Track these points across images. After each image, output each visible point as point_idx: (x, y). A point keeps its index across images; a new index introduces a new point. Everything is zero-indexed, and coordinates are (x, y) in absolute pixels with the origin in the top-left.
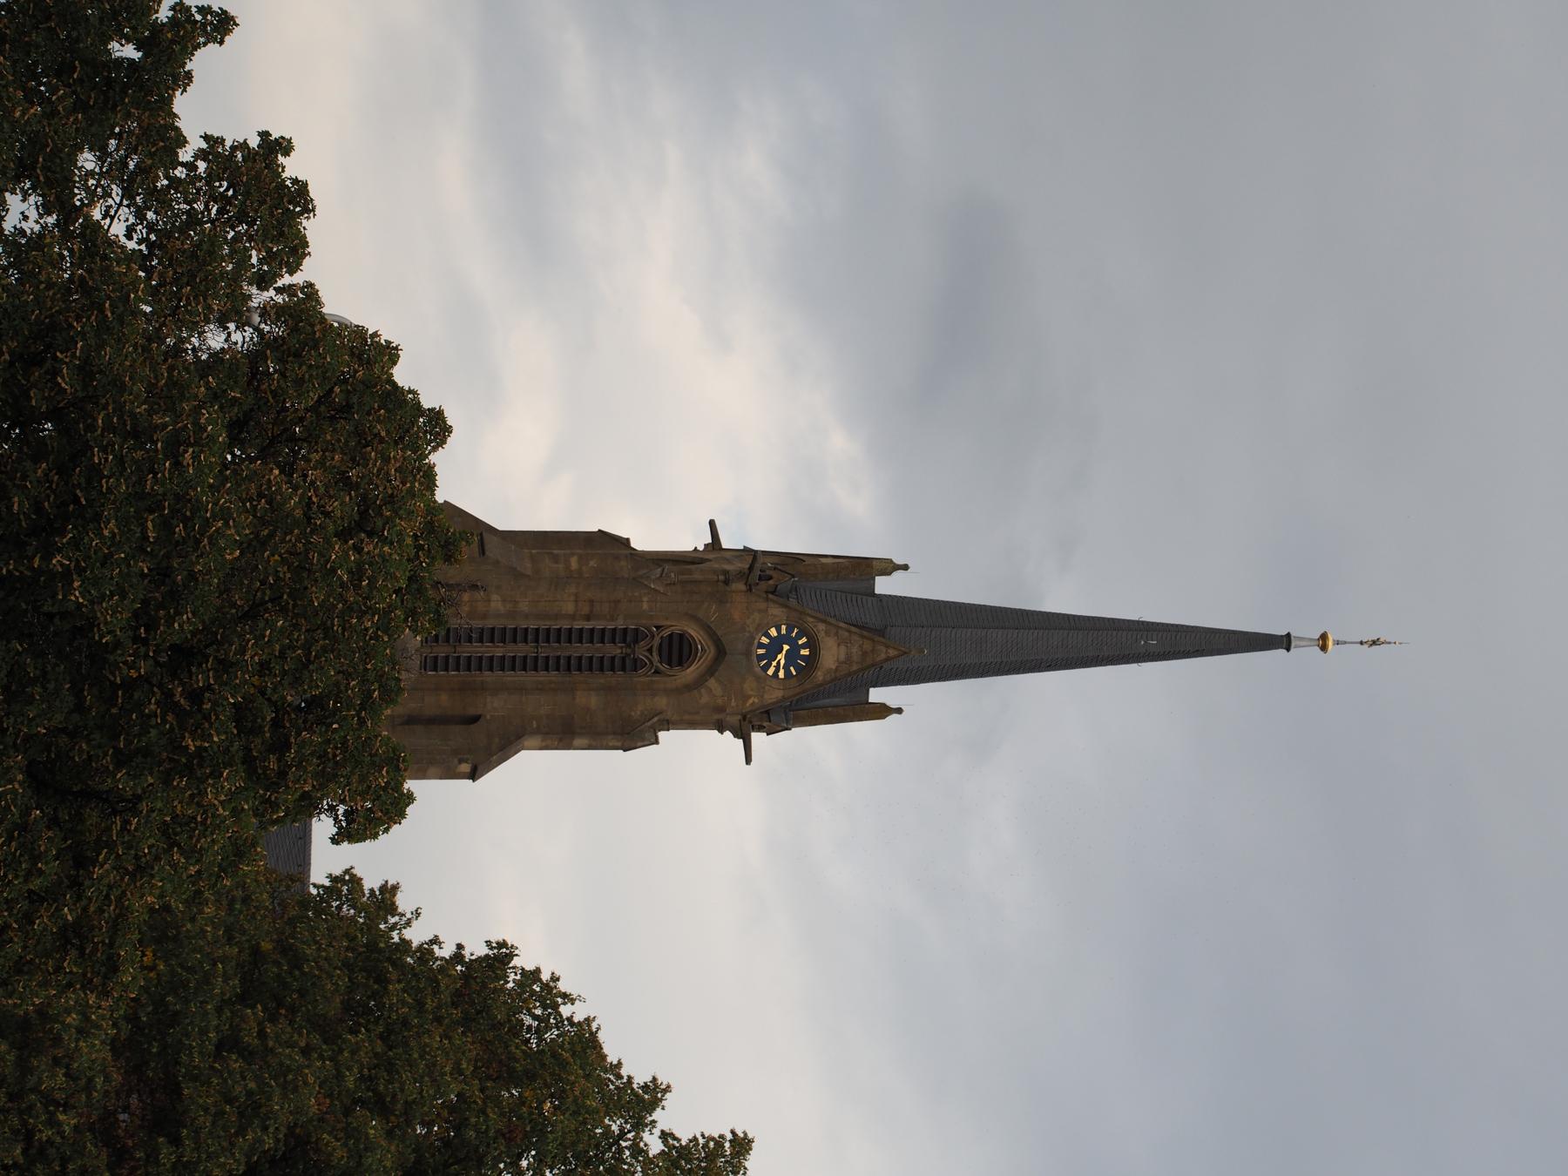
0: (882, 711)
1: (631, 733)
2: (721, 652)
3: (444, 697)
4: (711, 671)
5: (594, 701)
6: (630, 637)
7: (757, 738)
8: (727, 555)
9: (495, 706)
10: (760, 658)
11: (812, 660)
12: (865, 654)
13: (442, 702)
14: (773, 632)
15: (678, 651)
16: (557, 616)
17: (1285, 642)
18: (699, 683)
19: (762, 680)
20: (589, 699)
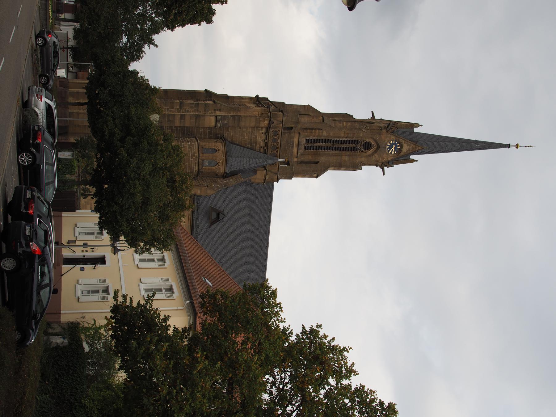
0: (413, 161)
1: (356, 167)
2: (378, 147)
3: (310, 157)
4: (376, 151)
5: (347, 158)
6: (356, 142)
7: (386, 168)
8: (378, 121)
9: (322, 159)
10: (388, 148)
11: (400, 150)
12: (413, 148)
13: (310, 158)
14: (391, 142)
15: (367, 146)
16: (340, 137)
17: (509, 146)
18: (373, 154)
19: (388, 154)
20: (345, 157)
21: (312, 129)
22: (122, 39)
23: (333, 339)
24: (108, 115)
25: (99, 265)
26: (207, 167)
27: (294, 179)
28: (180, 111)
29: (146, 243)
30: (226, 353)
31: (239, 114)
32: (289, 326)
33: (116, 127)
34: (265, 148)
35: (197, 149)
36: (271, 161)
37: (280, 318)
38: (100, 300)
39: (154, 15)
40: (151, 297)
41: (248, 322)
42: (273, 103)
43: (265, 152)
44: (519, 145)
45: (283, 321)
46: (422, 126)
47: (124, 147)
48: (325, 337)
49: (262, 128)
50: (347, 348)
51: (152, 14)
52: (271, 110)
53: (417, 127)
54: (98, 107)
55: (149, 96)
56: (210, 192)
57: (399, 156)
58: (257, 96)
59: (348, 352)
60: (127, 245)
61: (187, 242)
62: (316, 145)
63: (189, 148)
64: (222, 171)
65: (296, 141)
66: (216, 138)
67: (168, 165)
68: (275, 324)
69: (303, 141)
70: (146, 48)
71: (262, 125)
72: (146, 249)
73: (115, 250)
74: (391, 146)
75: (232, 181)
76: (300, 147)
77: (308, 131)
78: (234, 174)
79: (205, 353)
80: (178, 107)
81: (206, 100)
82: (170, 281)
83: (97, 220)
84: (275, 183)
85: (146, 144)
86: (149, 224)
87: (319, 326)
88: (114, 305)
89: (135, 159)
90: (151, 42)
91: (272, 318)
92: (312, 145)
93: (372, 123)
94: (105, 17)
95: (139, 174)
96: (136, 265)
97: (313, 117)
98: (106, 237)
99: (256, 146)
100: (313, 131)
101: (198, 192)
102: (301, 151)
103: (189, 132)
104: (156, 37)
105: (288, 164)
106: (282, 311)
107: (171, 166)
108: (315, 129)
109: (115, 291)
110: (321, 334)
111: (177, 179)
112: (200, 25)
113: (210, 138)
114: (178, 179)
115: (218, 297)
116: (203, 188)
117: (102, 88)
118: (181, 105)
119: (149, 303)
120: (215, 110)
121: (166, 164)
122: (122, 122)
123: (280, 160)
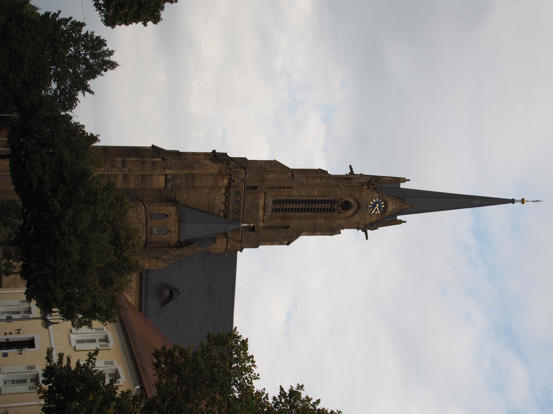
0: (400, 222)
1: (333, 231)
2: (359, 206)
3: (279, 221)
4: (356, 212)
5: (323, 221)
7: (369, 231)
9: (294, 223)
11: (385, 209)
12: (400, 207)
13: (279, 222)
14: (374, 201)
15: (346, 206)
17: (513, 201)
18: (353, 215)
19: (370, 214)
21: (280, 188)
22: (50, 85)
23: (318, 401)
25: (26, 349)
27: (260, 247)
29: (85, 315)
31: (193, 172)
32: (264, 389)
34: (226, 212)
35: (144, 214)
36: (232, 227)
37: (253, 374)
38: (28, 391)
39: (88, 57)
40: (94, 355)
42: (233, 159)
43: (226, 216)
44: (526, 199)
46: (409, 180)
47: (56, 197)
48: (308, 399)
49: (221, 188)
51: (86, 55)
52: (231, 167)
54: (23, 159)
57: (384, 216)
60: (62, 318)
61: (135, 320)
63: (136, 216)
64: (175, 239)
65: (261, 202)
67: (111, 218)
68: (246, 381)
69: (270, 202)
71: (221, 184)
73: (47, 324)
74: (374, 206)
75: (187, 251)
76: (266, 209)
77: (276, 190)
78: (189, 243)
80: (120, 166)
81: (154, 157)
83: (8, 162)
84: (239, 252)
87: (301, 387)
88: (48, 367)
89: (70, 210)
90: (86, 89)
91: (243, 375)
92: (281, 207)
93: (351, 179)
94: (29, 59)
96: (73, 347)
97: (281, 173)
98: (36, 311)
99: (214, 209)
100: (282, 190)
101: (147, 265)
102: (268, 214)
103: (134, 195)
105: (253, 229)
106: (254, 366)
108: (284, 188)
110: (303, 396)
111: (122, 234)
112: (145, 25)
114: (123, 234)
115: (177, 354)
116: (152, 261)
118: (124, 163)
119: (91, 362)
120: (164, 168)
121: (108, 217)
122: (53, 169)
123: (244, 225)
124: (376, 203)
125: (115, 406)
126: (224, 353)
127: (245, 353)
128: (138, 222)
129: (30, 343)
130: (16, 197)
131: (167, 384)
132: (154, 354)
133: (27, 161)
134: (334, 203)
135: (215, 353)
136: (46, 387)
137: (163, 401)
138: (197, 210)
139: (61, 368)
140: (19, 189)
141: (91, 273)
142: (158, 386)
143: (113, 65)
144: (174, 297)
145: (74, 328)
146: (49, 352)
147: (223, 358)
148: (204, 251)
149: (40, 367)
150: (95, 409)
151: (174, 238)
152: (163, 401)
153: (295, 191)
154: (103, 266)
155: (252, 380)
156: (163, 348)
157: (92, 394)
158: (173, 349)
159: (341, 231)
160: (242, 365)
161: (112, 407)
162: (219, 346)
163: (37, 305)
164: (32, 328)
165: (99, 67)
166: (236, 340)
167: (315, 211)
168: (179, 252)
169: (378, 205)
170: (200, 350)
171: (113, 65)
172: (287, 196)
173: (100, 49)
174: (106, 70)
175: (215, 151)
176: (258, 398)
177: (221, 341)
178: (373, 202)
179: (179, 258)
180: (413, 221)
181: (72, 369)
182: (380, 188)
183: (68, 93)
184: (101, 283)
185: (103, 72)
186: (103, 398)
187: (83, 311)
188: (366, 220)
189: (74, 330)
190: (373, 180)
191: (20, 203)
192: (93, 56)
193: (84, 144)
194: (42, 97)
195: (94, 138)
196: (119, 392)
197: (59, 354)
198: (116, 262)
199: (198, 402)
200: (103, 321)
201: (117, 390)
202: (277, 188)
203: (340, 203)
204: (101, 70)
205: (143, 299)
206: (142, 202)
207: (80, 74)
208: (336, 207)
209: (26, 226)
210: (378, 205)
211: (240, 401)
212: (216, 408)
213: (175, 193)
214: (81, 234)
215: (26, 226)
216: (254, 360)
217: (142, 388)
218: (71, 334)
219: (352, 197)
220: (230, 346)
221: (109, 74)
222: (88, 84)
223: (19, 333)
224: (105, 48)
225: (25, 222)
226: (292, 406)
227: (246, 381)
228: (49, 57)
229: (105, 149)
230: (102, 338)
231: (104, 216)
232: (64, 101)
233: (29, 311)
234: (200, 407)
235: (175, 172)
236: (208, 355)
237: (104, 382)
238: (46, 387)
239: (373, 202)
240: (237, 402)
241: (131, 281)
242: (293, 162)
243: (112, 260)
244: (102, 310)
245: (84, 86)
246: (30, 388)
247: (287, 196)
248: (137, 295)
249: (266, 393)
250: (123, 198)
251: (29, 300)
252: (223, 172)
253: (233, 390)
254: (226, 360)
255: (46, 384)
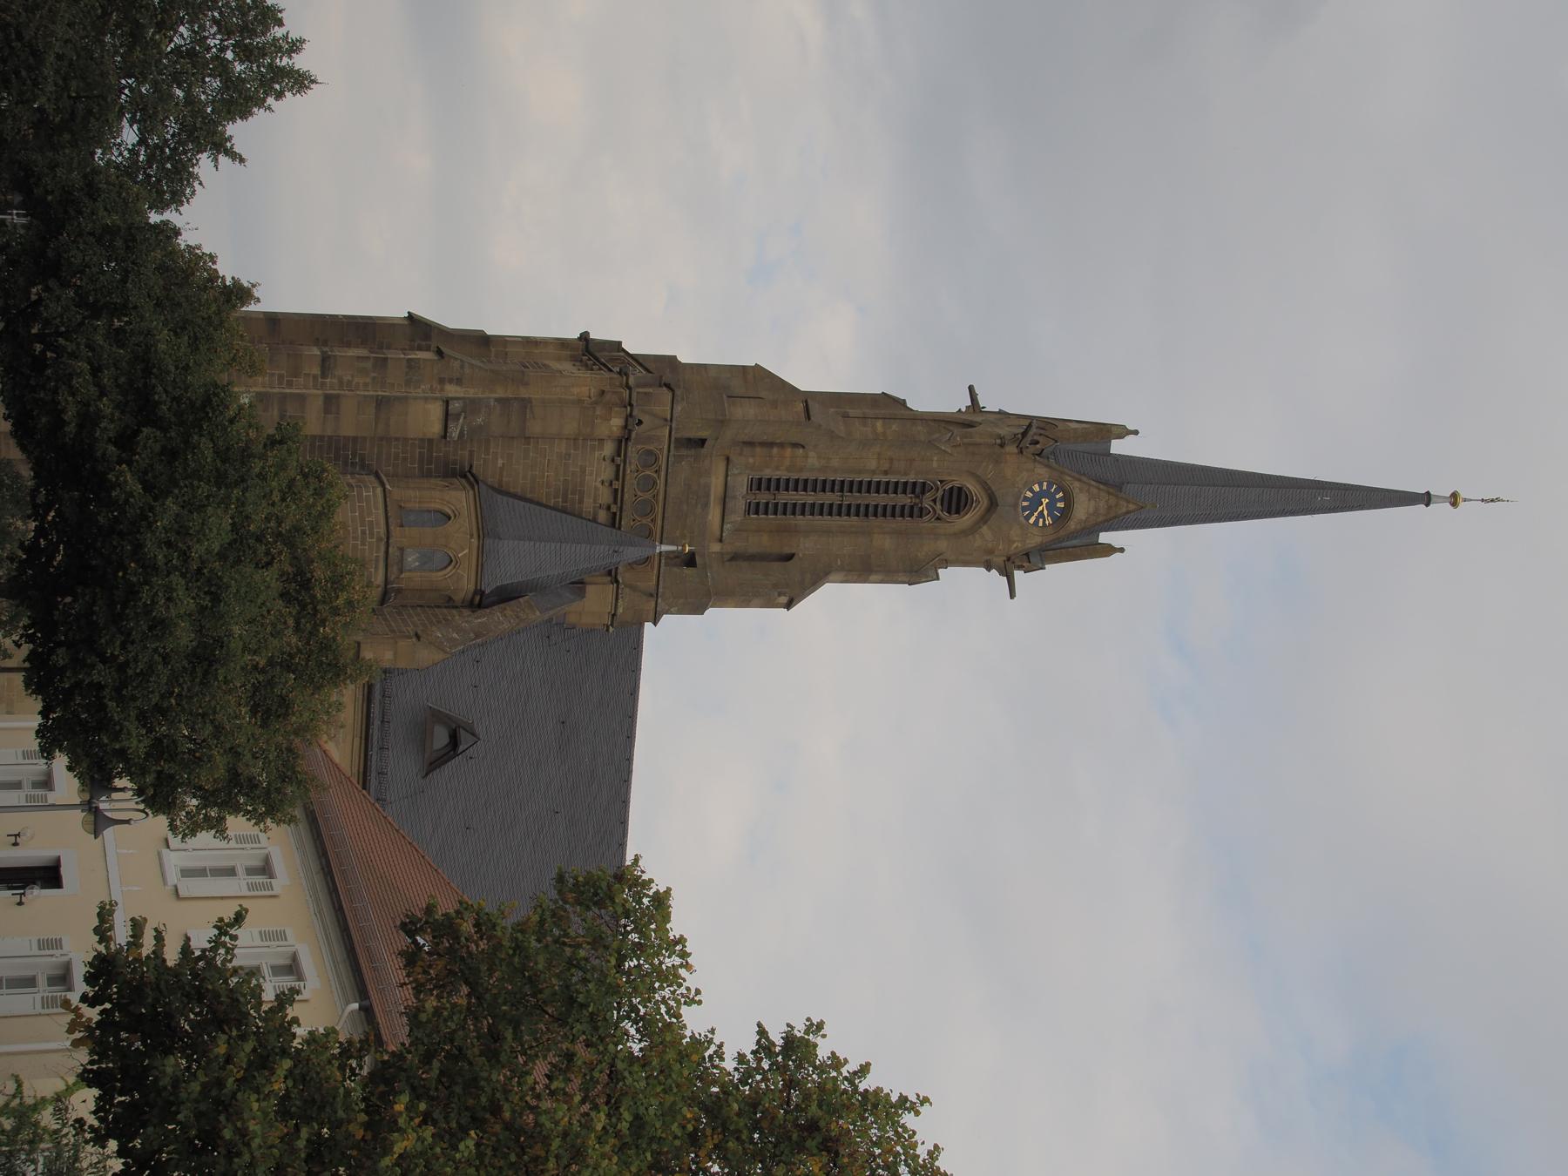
0: (1109, 550)
1: (917, 571)
2: (993, 504)
4: (984, 519)
5: (888, 543)
7: (1018, 574)
8: (992, 417)
9: (805, 546)
11: (1067, 512)
12: (1110, 508)
14: (1036, 488)
15: (956, 501)
17: (1427, 499)
20: (883, 538)
21: (771, 445)
22: (119, 131)
23: (864, 1070)
24: (73, 356)
26: (415, 572)
27: (710, 611)
28: (323, 384)
29: (208, 799)
30: (496, 1110)
31: (524, 393)
33: (102, 394)
34: (614, 509)
36: (632, 553)
37: (683, 990)
38: (39, 1009)
39: (229, 55)
40: (231, 925)
41: (571, 1001)
42: (637, 359)
43: (614, 522)
44: (1463, 495)
45: (693, 1001)
46: (1136, 432)
47: (129, 463)
48: (836, 1062)
49: (601, 440)
50: (913, 1098)
51: (223, 49)
52: (632, 381)
53: (1120, 437)
54: (38, 347)
55: (219, 312)
56: (426, 656)
57: (1062, 533)
58: (584, 337)
59: (917, 1113)
60: (142, 806)
62: (785, 497)
63: (358, 518)
65: (716, 484)
66: (445, 476)
67: (286, 526)
68: (663, 1009)
69: (741, 484)
70: (204, 165)
72: (207, 818)
73: (98, 822)
75: (499, 619)
76: (730, 505)
77: (758, 450)
78: (506, 596)
79: (423, 1106)
80: (316, 371)
81: (412, 349)
82: (291, 940)
83: (35, 721)
84: (648, 626)
85: (209, 454)
86: (218, 730)
87: (816, 1028)
88: (99, 956)
89: (169, 501)
90: (220, 146)
91: (655, 990)
92: (773, 498)
93: (970, 425)
94: (59, 57)
95: (185, 556)
96: (170, 888)
98: (67, 786)
99: (581, 501)
100: (775, 450)
101: (387, 657)
103: (354, 455)
104: (237, 131)
105: (690, 561)
106: (687, 966)
107: (297, 529)
108: (782, 445)
109: (102, 907)
110: (823, 1053)
111: (318, 574)
113: (427, 474)
114: (320, 572)
115: (467, 927)
116: (402, 643)
117: (52, 283)
118: (326, 363)
119: (224, 945)
120: (442, 381)
123: (665, 548)
124: (1042, 494)
125: (290, 1072)
126: (604, 928)
127: (662, 930)
128: (363, 532)
129: (49, 875)
130: (14, 453)
131: (437, 1012)
132: (403, 926)
133: (49, 354)
134: (923, 493)
135: (576, 927)
136: (93, 1014)
137: (427, 1059)
138: (530, 501)
139: (137, 960)
140: (23, 432)
141: (226, 682)
142: (413, 1016)
143: (301, 82)
144: (461, 748)
145: (176, 835)
146: (105, 914)
147: (597, 942)
148: (550, 620)
149: (81, 951)
150: (231, 1080)
151: (464, 582)
152: (427, 1059)
153: (812, 454)
154: (262, 663)
155: (679, 1007)
156: (429, 910)
157: (224, 1037)
158: (458, 912)
159: (940, 571)
160: (652, 964)
161: (281, 1073)
162: (588, 908)
163: (70, 768)
164: (53, 833)
165: (262, 85)
166: (638, 893)
167: (866, 515)
168: (480, 619)
169: (1045, 501)
170: (536, 918)
171: (301, 82)
172: (788, 470)
173: (264, 34)
174: (279, 96)
175: (587, 333)
176: (695, 1058)
177: (596, 894)
178: (1031, 490)
179: (477, 636)
180: (1140, 546)
181: (170, 963)
182: (1053, 453)
183: (169, 158)
184: (254, 712)
185: (270, 100)
186: (254, 1050)
187: (200, 788)
188: (1011, 542)
189: (175, 842)
190: (1034, 430)
191: (26, 472)
192: (246, 53)
193: (214, 308)
194: (96, 171)
195: (240, 293)
196: (301, 1031)
197: (133, 920)
198: (300, 651)
199: (526, 1063)
200: (260, 819)
201: (295, 1029)
202: (763, 444)
203: (940, 493)
204: (267, 94)
205: (374, 753)
206: (378, 476)
207: (206, 104)
208: (927, 503)
209: (42, 542)
210: (1045, 501)
211: (644, 1066)
212: (577, 1082)
213: (471, 453)
214: (199, 570)
215: (42, 542)
216: (688, 950)
217: (367, 1011)
218: (165, 851)
219: (973, 475)
220: (620, 910)
221: (287, 109)
222: (228, 133)
223: (16, 844)
224: (278, 32)
225: (40, 532)
226: (791, 1081)
227: (663, 1009)
228: (116, 53)
229: (274, 321)
230: (257, 863)
231: (267, 519)
232: (159, 181)
233: (47, 783)
234: (530, 1080)
235: (471, 393)
236: (556, 932)
237: (260, 1003)
238: (93, 1014)
239: (1031, 490)
240: (636, 1068)
241: (339, 706)
242: (806, 376)
243: (289, 644)
244: (256, 786)
245: (216, 139)
246: (46, 1003)
247: (788, 470)
248: (357, 740)
249: (717, 1041)
250: (324, 470)
251: (47, 752)
252: (608, 397)
253: (626, 1033)
254: (606, 947)
255: (92, 1005)
